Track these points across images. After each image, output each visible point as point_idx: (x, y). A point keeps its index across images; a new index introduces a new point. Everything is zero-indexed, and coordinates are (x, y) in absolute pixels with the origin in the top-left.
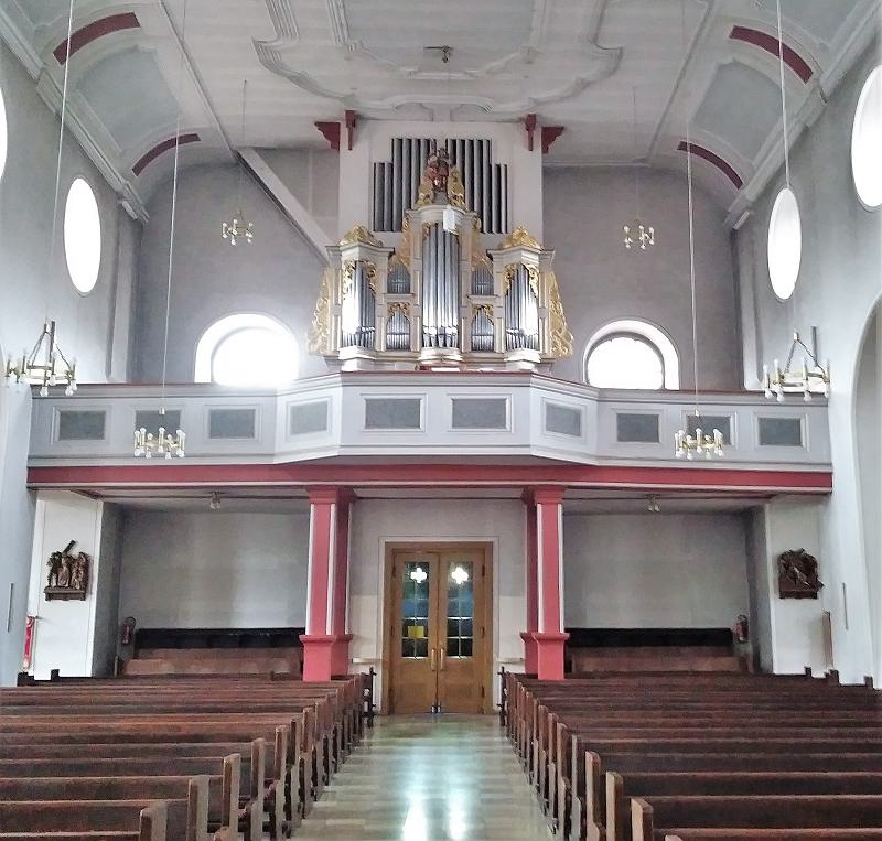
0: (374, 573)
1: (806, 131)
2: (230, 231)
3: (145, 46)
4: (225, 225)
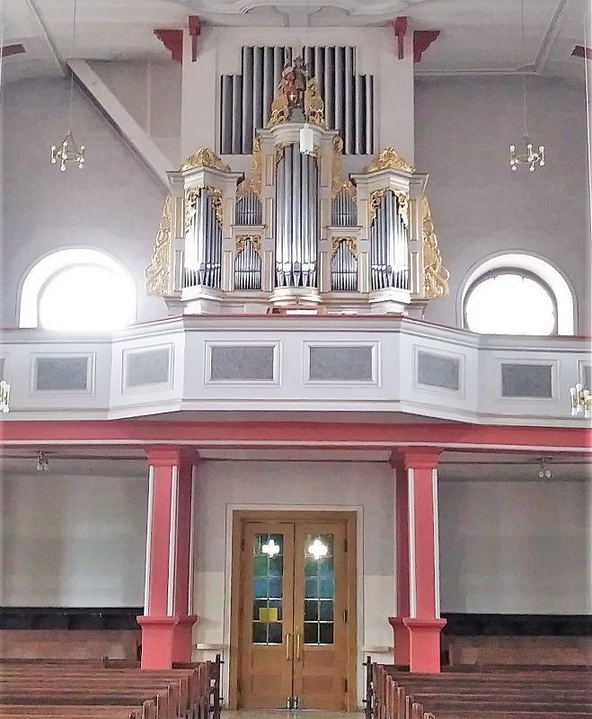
0: (220, 545)
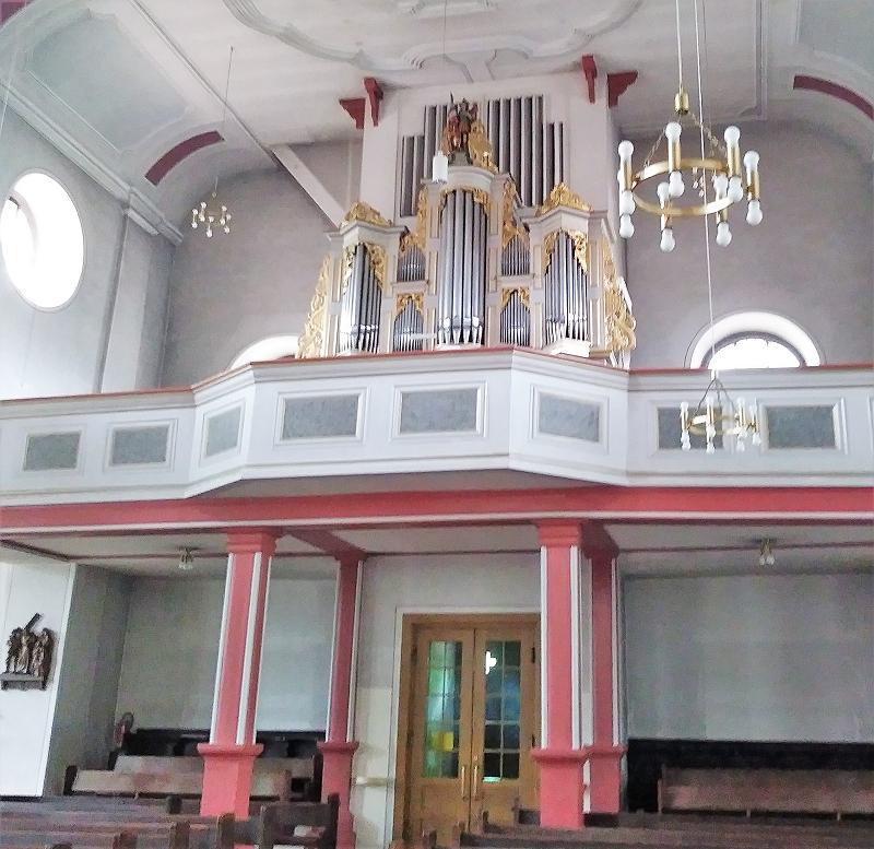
0: (388, 656)
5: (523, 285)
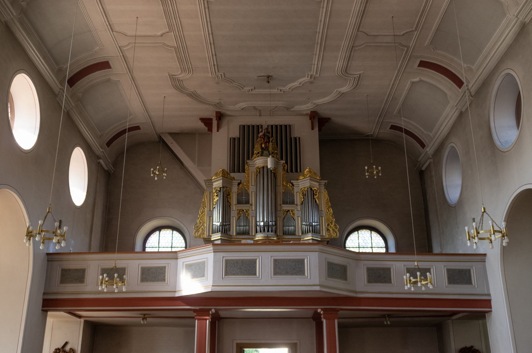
1: (461, 115)
2: (155, 173)
3: (114, 78)
4: (152, 169)
5: (293, 208)
